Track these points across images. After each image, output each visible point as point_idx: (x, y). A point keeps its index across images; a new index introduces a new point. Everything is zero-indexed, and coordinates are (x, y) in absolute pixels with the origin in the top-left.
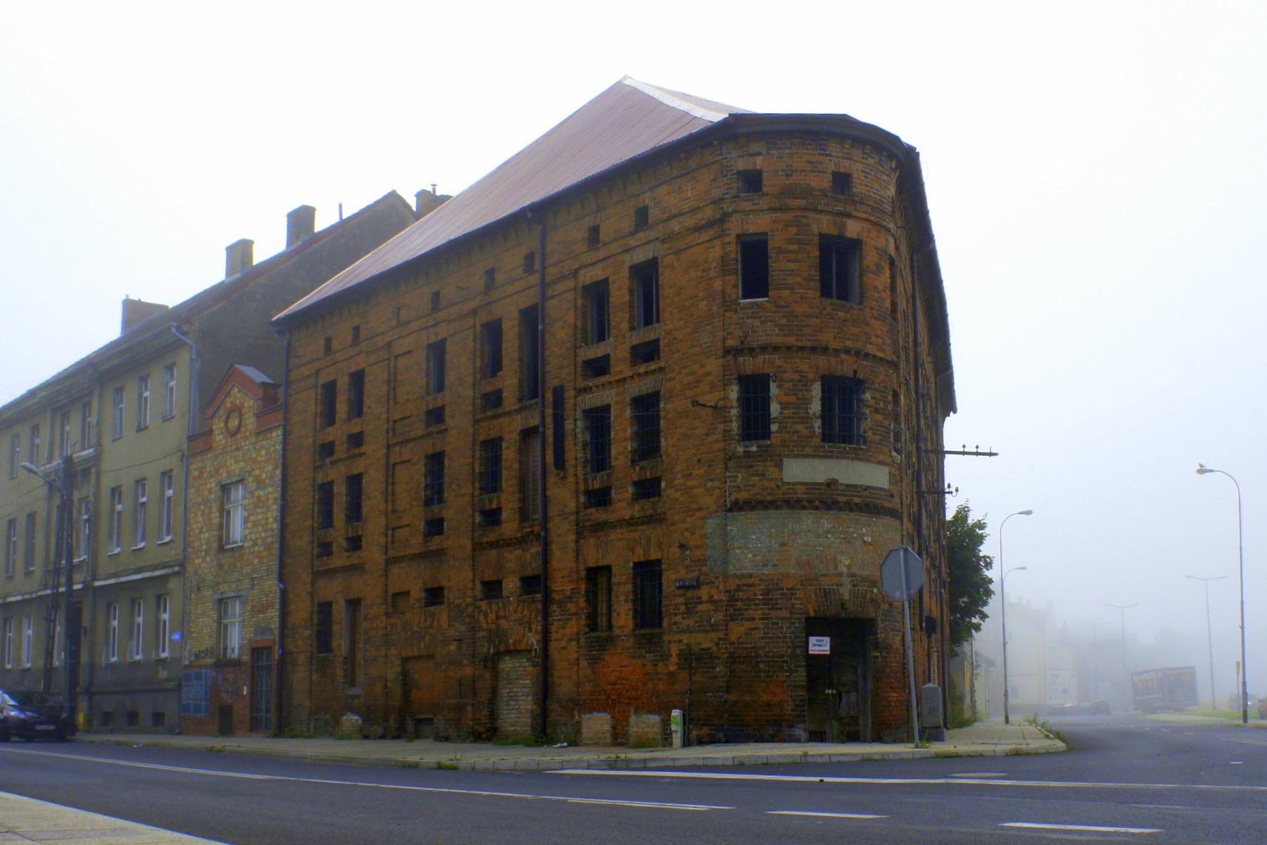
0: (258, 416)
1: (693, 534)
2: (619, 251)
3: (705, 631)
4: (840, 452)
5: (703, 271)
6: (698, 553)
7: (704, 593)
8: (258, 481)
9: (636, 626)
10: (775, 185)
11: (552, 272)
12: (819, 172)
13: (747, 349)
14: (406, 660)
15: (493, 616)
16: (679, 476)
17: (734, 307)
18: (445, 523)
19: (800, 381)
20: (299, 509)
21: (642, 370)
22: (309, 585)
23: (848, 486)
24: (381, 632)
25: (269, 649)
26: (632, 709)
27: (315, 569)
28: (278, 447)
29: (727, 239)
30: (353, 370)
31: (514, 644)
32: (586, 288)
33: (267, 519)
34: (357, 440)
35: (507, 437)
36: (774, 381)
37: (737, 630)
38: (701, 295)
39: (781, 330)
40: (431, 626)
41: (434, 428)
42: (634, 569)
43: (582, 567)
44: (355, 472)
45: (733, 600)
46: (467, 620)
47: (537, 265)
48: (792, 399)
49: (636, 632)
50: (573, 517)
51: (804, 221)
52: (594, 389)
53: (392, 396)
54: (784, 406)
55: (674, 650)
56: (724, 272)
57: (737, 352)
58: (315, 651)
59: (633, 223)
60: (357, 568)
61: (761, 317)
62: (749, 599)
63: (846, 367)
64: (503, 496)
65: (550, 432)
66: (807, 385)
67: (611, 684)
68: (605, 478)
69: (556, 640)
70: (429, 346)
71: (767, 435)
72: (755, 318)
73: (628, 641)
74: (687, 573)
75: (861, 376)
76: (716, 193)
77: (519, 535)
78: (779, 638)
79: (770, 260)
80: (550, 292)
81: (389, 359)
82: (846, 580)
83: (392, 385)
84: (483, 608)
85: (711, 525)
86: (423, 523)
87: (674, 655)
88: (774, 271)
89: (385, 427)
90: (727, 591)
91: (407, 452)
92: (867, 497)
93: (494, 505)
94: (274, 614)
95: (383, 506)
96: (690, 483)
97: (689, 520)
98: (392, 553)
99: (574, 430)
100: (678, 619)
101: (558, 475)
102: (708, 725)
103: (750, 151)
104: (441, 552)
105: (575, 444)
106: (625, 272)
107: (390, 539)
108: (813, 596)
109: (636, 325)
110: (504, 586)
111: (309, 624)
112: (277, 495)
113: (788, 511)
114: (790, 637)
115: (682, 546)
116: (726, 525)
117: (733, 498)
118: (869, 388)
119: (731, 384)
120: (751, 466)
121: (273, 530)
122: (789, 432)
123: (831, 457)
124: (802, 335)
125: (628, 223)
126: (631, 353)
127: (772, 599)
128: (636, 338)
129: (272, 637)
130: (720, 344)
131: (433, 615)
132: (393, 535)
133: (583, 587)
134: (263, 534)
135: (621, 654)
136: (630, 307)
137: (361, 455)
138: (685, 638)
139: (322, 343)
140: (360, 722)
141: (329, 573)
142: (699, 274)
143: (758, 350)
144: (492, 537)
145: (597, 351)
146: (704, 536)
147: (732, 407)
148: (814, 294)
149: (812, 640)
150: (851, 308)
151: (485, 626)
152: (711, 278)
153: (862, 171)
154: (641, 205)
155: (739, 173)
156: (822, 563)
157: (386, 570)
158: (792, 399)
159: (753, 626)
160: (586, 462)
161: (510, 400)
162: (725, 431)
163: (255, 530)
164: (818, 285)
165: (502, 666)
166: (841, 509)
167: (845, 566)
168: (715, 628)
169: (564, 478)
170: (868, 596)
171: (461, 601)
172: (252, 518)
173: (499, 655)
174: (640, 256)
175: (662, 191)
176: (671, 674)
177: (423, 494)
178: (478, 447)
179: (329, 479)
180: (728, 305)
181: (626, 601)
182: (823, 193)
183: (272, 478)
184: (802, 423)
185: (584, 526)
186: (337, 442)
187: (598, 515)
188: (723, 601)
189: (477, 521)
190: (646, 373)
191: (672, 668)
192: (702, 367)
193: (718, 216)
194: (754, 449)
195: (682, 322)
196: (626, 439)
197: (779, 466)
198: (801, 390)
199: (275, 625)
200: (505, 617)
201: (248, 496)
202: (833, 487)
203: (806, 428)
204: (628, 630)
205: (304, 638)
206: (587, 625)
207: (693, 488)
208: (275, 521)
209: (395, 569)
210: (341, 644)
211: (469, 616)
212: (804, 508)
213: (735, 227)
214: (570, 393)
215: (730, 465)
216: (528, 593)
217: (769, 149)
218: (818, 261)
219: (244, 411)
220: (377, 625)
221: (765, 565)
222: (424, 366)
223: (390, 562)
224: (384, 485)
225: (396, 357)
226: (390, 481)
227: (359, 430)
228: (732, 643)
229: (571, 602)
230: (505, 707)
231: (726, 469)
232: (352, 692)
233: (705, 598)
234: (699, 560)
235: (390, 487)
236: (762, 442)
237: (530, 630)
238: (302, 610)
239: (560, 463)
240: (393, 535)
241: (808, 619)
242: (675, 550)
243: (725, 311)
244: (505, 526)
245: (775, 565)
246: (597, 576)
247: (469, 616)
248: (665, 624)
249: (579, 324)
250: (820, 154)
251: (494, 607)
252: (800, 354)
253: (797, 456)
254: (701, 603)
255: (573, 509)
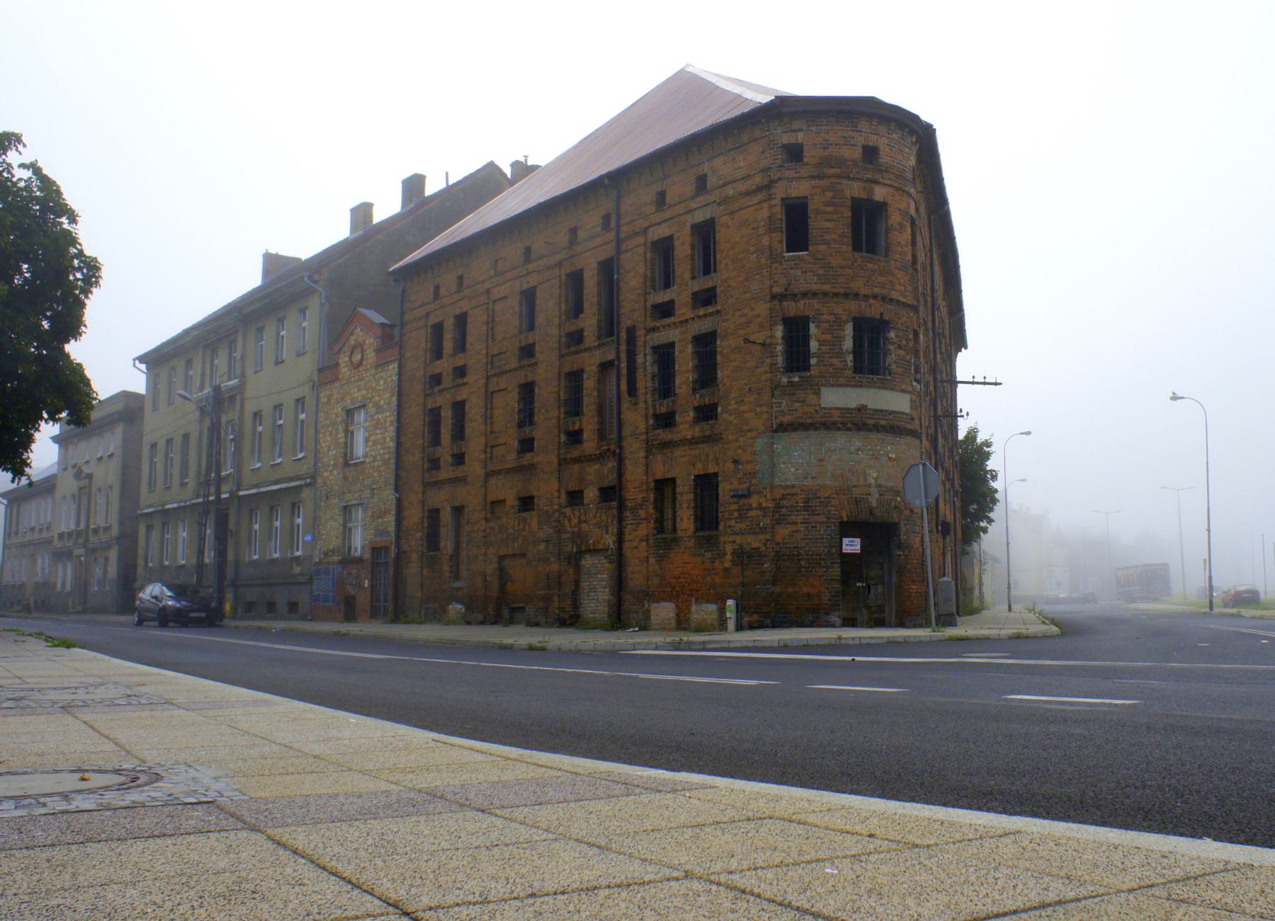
0: (378, 351)
1: (744, 451)
2: (683, 212)
3: (755, 533)
4: (869, 382)
5: (754, 229)
6: (749, 467)
7: (754, 501)
8: (377, 406)
9: (697, 529)
10: (814, 156)
11: (626, 230)
12: (852, 145)
13: (792, 295)
14: (502, 558)
15: (576, 521)
16: (733, 402)
17: (779, 259)
18: (535, 442)
19: (835, 322)
20: (412, 430)
21: (701, 312)
22: (420, 495)
23: (875, 410)
24: (481, 534)
25: (387, 548)
26: (693, 600)
27: (426, 481)
28: (394, 378)
29: (773, 202)
30: (458, 312)
31: (594, 544)
32: (655, 244)
33: (385, 438)
34: (461, 372)
35: (587, 369)
36: (814, 322)
37: (782, 532)
38: (752, 249)
39: (818, 279)
40: (524, 530)
41: (526, 362)
42: (695, 480)
43: (651, 479)
44: (459, 399)
45: (778, 507)
46: (554, 524)
47: (613, 224)
48: (828, 337)
49: (697, 534)
50: (644, 437)
51: (839, 186)
52: (661, 329)
53: (490, 336)
54: (822, 343)
55: (729, 549)
56: (771, 229)
57: (781, 297)
58: (425, 550)
59: (694, 189)
60: (462, 480)
61: (802, 268)
62: (792, 506)
63: (874, 310)
64: (585, 419)
65: (624, 365)
66: (841, 326)
67: (675, 578)
68: (670, 404)
69: (629, 541)
70: (522, 292)
71: (807, 367)
72: (797, 268)
73: (690, 541)
74: (740, 484)
75: (886, 317)
76: (764, 163)
77: (598, 452)
78: (817, 539)
79: (809, 220)
80: (624, 247)
81: (488, 303)
82: (874, 490)
83: (490, 325)
84: (568, 514)
85: (760, 443)
86: (517, 442)
87: (729, 553)
88: (814, 229)
89: (485, 361)
90: (773, 500)
91: (503, 382)
92: (892, 420)
93: (577, 427)
94: (391, 518)
95: (482, 427)
96: (742, 408)
97: (741, 439)
98: (490, 467)
99: (644, 363)
100: (732, 523)
101: (631, 401)
102: (757, 613)
103: (793, 128)
104: (532, 467)
105: (645, 376)
106: (688, 230)
107: (489, 455)
108: (846, 503)
109: (696, 275)
110: (585, 495)
111: (420, 527)
112: (394, 418)
113: (825, 432)
114: (827, 538)
115: (735, 462)
116: (773, 444)
117: (778, 421)
118: (893, 328)
119: (775, 324)
120: (795, 394)
121: (389, 448)
122: (825, 365)
123: (861, 386)
124: (837, 283)
125: (689, 189)
126: (692, 298)
127: (811, 506)
128: (697, 286)
129: (389, 538)
130: (767, 290)
131: (525, 520)
132: (491, 452)
133: (652, 496)
134: (381, 451)
135: (684, 552)
136: (692, 259)
137: (464, 384)
138: (738, 539)
139: (432, 289)
140: (463, 610)
141: (438, 484)
142: (750, 231)
143: (799, 296)
144: (575, 454)
145: (663, 297)
146: (754, 453)
147: (777, 344)
148: (847, 248)
149: (846, 541)
150: (879, 260)
151: (569, 529)
152: (760, 236)
153: (888, 145)
154: (701, 173)
155: (784, 146)
156: (854, 476)
157: (486, 482)
158: (828, 337)
159: (795, 529)
160: (654, 390)
161: (590, 338)
162: (772, 364)
163: (375, 448)
164: (850, 242)
165: (583, 563)
166: (870, 430)
167: (873, 478)
168: (763, 530)
169: (636, 404)
170: (893, 504)
171: (548, 508)
172: (372, 438)
173: (581, 553)
174: (700, 217)
175: (718, 162)
176: (726, 570)
177: (517, 417)
178: (563, 378)
179: (437, 405)
180: (774, 258)
181: (688, 508)
182: (855, 164)
183: (389, 403)
184: (837, 357)
185: (653, 445)
186: (444, 374)
187: (664, 435)
188: (769, 508)
189: (562, 440)
190: (705, 315)
191: (727, 564)
192: (752, 310)
193: (766, 183)
194: (796, 379)
195: (735, 272)
196: (688, 371)
197: (818, 394)
198: (836, 330)
199: (392, 528)
200: (585, 522)
201: (368, 419)
202: (863, 411)
203: (841, 362)
204: (689, 533)
205: (416, 540)
206: (655, 528)
207: (745, 412)
208: (392, 440)
209: (493, 481)
210: (447, 544)
211: (555, 521)
212: (839, 429)
213: (780, 192)
214: (641, 332)
215: (776, 393)
216: (605, 501)
217: (809, 126)
218: (850, 220)
219: (365, 347)
220: (478, 529)
221: (806, 478)
222: (517, 309)
223: (488, 475)
224: (483, 410)
225: (494, 302)
226: (489, 407)
227: (463, 364)
228: (777, 544)
229: (642, 509)
230: (586, 598)
231: (773, 396)
232: (457, 584)
233: (755, 505)
234: (750, 473)
235: (489, 412)
236: (803, 374)
237: (607, 533)
238: (414, 516)
239: (632, 391)
240: (491, 452)
241: (842, 523)
242: (729, 465)
243: (772, 263)
244: (586, 445)
245: (814, 478)
246: (664, 487)
247: (555, 521)
248: (721, 527)
249: (649, 274)
250: (851, 130)
251: (577, 513)
252: (835, 299)
253: (833, 386)
254: (752, 509)
255: (644, 430)
